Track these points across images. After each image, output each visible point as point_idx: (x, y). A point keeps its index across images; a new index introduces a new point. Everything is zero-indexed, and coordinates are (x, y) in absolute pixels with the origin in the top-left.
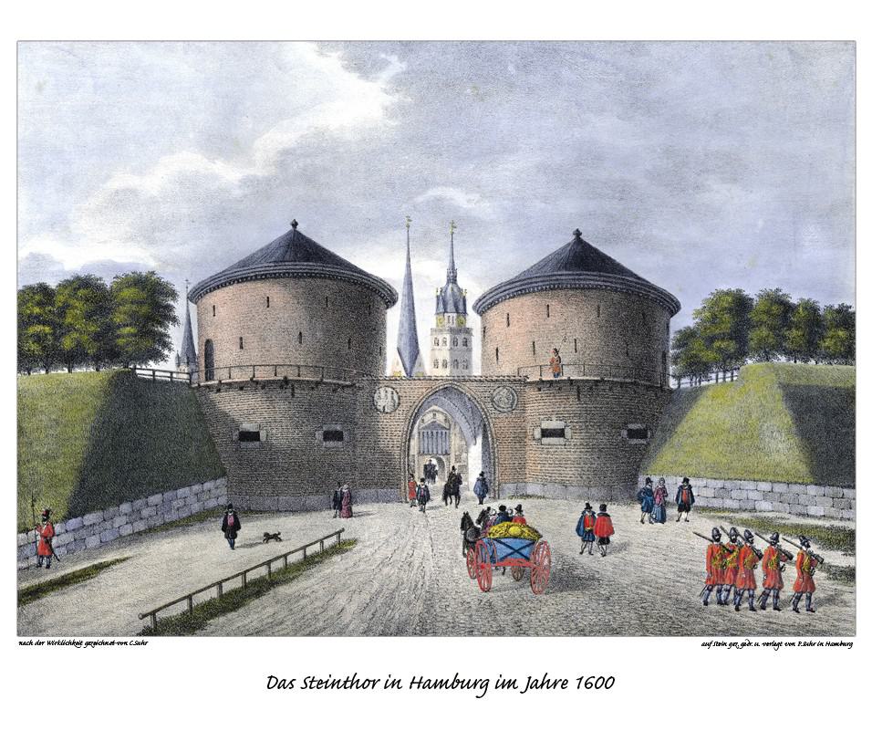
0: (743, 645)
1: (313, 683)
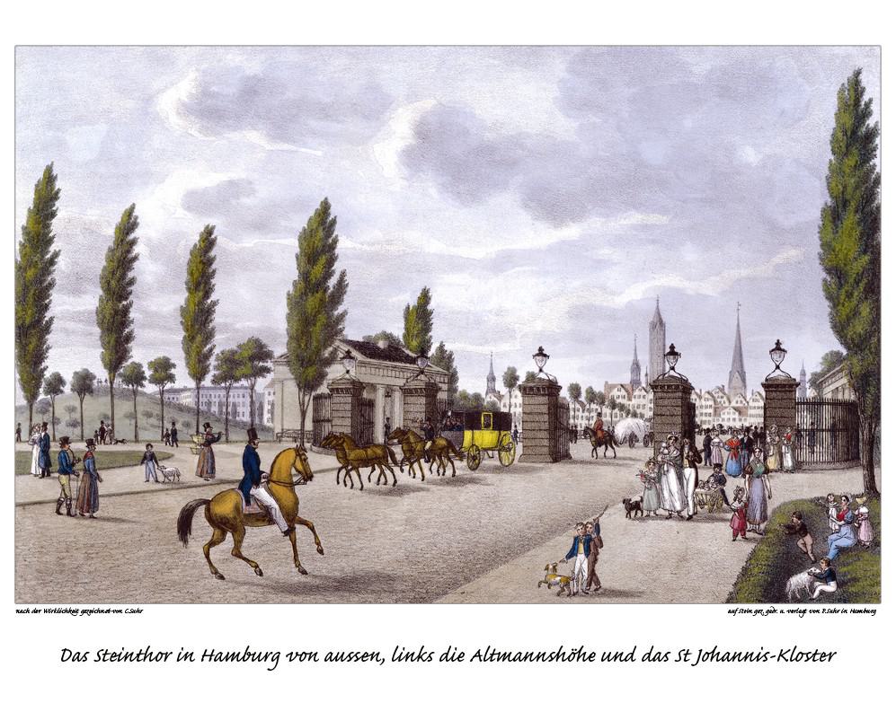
0: (769, 612)
1: (103, 656)
